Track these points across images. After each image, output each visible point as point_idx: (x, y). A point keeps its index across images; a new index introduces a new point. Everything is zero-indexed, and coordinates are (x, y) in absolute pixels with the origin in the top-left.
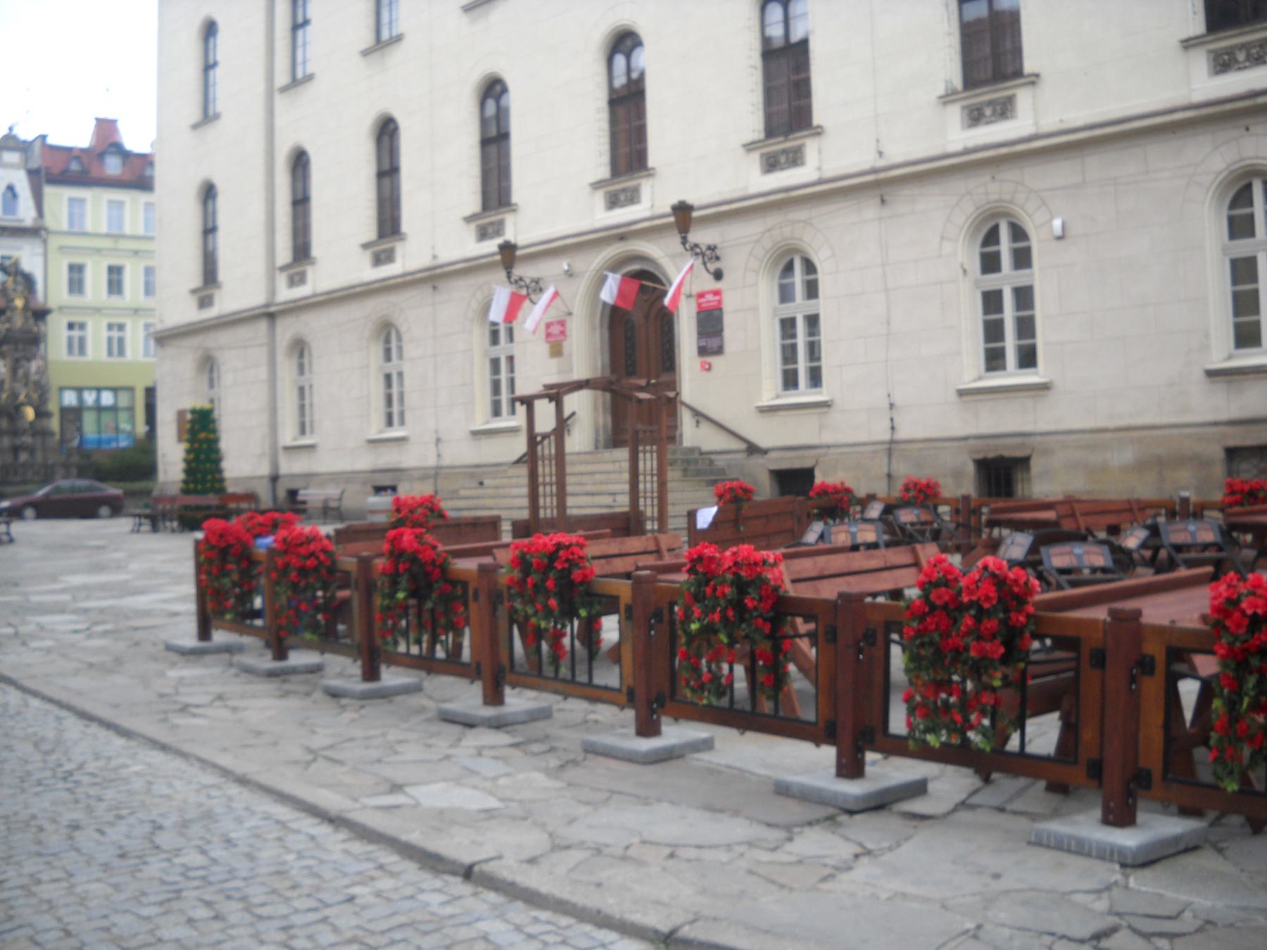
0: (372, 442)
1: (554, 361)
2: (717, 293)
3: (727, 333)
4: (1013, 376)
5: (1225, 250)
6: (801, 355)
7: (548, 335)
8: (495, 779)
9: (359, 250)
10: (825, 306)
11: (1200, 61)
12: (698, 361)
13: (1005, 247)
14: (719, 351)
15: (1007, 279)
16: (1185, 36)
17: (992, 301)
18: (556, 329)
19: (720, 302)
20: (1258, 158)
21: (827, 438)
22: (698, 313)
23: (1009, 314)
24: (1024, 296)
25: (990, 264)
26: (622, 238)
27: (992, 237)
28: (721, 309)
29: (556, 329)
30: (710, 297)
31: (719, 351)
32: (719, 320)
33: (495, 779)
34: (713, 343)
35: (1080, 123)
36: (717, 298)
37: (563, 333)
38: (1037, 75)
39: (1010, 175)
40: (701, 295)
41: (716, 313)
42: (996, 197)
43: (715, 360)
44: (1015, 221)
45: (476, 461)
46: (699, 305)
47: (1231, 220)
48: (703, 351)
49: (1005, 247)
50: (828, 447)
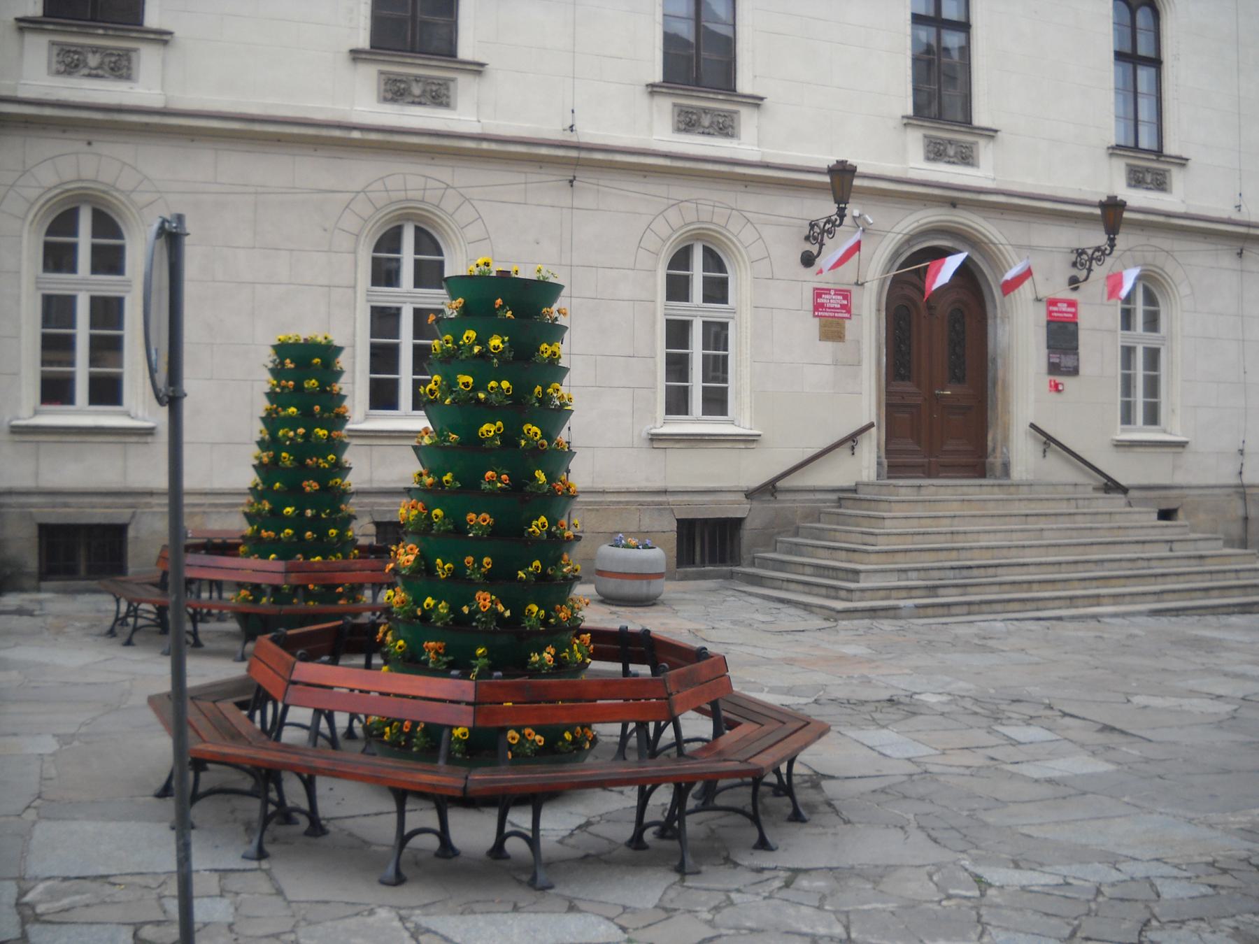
0: (17, 430)
1: (829, 346)
2: (1072, 304)
3: (1082, 350)
4: (696, 423)
5: (38, 281)
6: (1143, 387)
7: (818, 307)
8: (940, 901)
9: (642, 99)
10: (662, 309)
11: (915, 141)
12: (1046, 380)
13: (84, 241)
14: (1074, 371)
15: (83, 284)
16: (354, 47)
17: (678, 332)
18: (834, 301)
19: (1075, 314)
20: (83, 181)
21: (1179, 479)
22: (1049, 322)
23: (696, 351)
24: (717, 334)
25: (677, 289)
26: (954, 204)
27: (64, 222)
28: (1076, 324)
29: (834, 301)
30: (1063, 307)
31: (1074, 371)
32: (1074, 336)
33: (940, 901)
34: (1067, 361)
35: (894, 174)
36: (1073, 310)
37: (846, 308)
38: (482, 65)
39: (443, 173)
40: (1053, 302)
41: (1071, 327)
42: (418, 195)
43: (1067, 382)
44: (98, 207)
45: (658, 484)
46: (1050, 313)
47: (48, 247)
48: (1054, 369)
49: (84, 241)
50: (1182, 487)
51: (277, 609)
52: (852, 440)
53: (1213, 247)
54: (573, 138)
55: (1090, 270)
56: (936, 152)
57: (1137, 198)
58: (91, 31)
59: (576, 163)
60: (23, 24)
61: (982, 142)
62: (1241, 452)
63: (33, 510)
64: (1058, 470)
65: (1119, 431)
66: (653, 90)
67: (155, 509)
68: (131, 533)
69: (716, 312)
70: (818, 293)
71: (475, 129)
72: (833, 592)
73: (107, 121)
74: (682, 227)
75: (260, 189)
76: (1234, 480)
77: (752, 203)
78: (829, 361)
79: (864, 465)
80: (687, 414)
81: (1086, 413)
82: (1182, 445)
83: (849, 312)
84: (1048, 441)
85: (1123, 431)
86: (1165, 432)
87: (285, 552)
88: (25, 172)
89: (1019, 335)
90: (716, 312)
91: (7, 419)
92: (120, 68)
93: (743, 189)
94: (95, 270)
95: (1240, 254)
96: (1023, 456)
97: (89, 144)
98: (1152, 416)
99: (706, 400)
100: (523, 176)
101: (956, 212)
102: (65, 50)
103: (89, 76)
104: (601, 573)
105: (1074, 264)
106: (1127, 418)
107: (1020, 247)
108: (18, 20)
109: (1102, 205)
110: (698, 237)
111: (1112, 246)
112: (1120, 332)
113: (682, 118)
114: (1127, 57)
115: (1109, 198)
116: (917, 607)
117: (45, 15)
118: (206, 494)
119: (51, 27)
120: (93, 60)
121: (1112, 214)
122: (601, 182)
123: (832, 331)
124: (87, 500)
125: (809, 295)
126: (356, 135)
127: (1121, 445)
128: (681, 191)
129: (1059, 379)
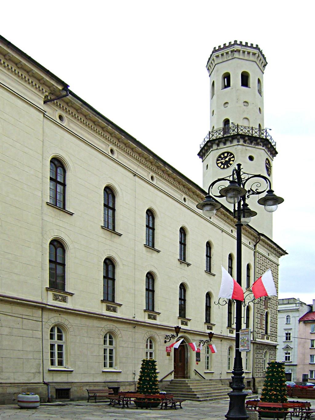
1: (168, 356)
7: (167, 350)
19: (200, 351)
39: (65, 316)
43: (199, 363)
48: (197, 361)
51: (148, 401)
52: (171, 373)
53: (217, 340)
54: (135, 319)
55: (170, 340)
56: (108, 309)
57: (183, 327)
58: (60, 292)
59: (136, 324)
60: (47, 289)
61: (118, 307)
62: (221, 374)
63: (55, 386)
64: (197, 377)
65: (50, 367)
66: (47, 289)
67: (75, 386)
68: (71, 390)
69: (60, 343)
70: (167, 348)
71: (72, 308)
72: (194, 398)
73: (88, 315)
74: (57, 322)
75: (88, 326)
76: (219, 378)
77: (158, 332)
78: (168, 359)
79: (172, 377)
80: (62, 366)
81: (201, 368)
82: (213, 373)
83: (171, 351)
84: (196, 372)
85: (51, 367)
86: (210, 370)
87: (145, 392)
88: (49, 320)
89: (192, 355)
90: (60, 343)
91: (48, 368)
92: (64, 300)
93: (54, 312)
94: (58, 339)
95: (221, 341)
96: (193, 375)
97: (60, 315)
98: (60, 363)
99: (58, 362)
100: (127, 326)
101: (185, 334)
102: (55, 295)
103: (59, 301)
104: (19, 401)
105: (166, 338)
106: (52, 363)
107: (193, 340)
108: (46, 288)
109: (175, 327)
110: (56, 325)
111: (211, 340)
112: (50, 340)
113: (55, 297)
114: (185, 300)
115: (210, 332)
116: (209, 399)
117: (50, 287)
118: (81, 383)
119: (54, 290)
120: (60, 298)
121: (177, 329)
122: (140, 328)
123: (169, 354)
124: (62, 384)
125: (165, 348)
126: (105, 317)
127: (205, 373)
128: (149, 329)
129: (198, 362)
